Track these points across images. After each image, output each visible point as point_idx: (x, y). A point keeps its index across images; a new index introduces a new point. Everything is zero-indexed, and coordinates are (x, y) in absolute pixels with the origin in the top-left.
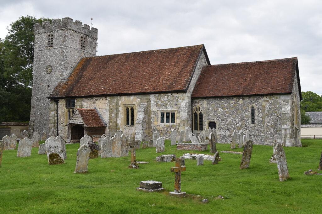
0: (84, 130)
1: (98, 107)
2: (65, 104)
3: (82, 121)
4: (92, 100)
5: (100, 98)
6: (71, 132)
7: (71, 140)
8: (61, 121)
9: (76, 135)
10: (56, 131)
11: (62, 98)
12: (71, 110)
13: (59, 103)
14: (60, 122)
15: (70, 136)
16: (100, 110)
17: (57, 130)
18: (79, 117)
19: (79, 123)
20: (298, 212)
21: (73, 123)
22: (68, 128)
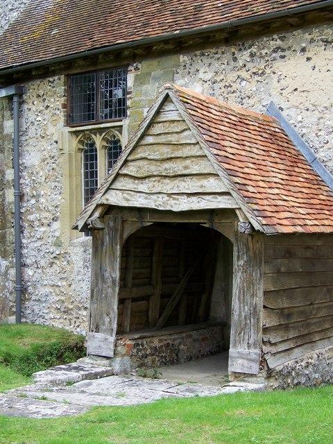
0: (239, 263)
1: (295, 99)
2: (64, 106)
3: (211, 185)
4: (244, 56)
5: (307, 36)
6: (117, 275)
7: (121, 332)
8: (39, 209)
9: (146, 298)
10: (13, 272)
11: (43, 71)
12: (98, 141)
13: (25, 107)
14: (31, 217)
15: (109, 305)
16: (312, 118)
17: (21, 266)
18: (186, 151)
19: (183, 205)
20: (86, 441)
21: (139, 202)
22: (97, 247)
